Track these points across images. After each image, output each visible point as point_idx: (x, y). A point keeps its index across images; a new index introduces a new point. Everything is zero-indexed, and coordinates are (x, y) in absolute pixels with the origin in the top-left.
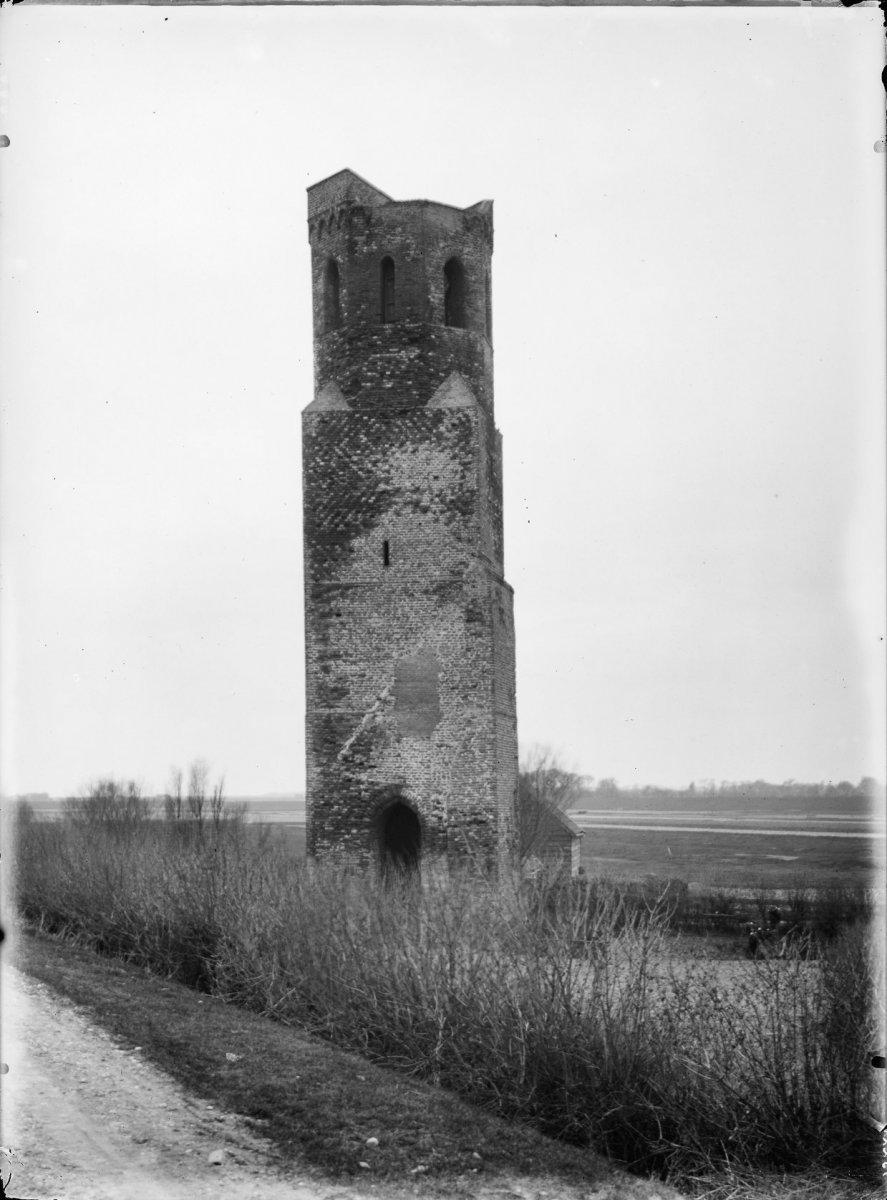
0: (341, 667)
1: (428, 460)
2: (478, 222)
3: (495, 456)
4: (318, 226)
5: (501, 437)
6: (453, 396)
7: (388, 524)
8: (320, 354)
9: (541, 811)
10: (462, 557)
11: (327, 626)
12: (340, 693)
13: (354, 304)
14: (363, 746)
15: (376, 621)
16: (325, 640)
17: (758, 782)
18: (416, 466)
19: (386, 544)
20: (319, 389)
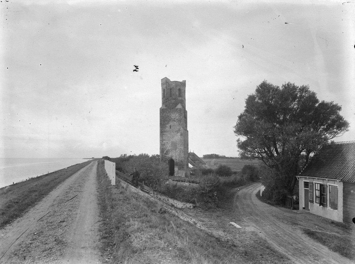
0: (164, 142)
1: (176, 115)
2: (183, 84)
3: (186, 114)
4: (162, 84)
5: (187, 112)
6: (179, 106)
7: (171, 123)
8: (162, 101)
9: (193, 158)
10: (180, 127)
11: (163, 136)
12: (164, 145)
13: (167, 94)
14: (167, 152)
15: (169, 135)
16: (162, 138)
17: (304, 89)
18: (175, 116)
19: (170, 126)
20: (162, 106)
